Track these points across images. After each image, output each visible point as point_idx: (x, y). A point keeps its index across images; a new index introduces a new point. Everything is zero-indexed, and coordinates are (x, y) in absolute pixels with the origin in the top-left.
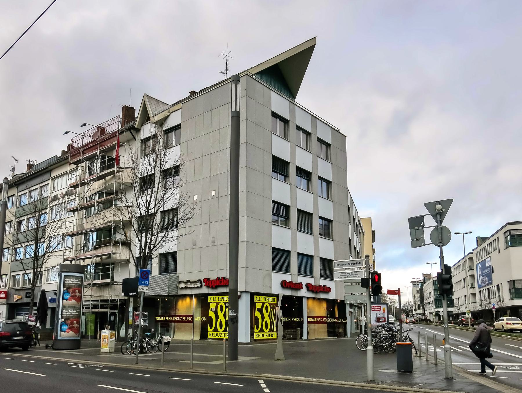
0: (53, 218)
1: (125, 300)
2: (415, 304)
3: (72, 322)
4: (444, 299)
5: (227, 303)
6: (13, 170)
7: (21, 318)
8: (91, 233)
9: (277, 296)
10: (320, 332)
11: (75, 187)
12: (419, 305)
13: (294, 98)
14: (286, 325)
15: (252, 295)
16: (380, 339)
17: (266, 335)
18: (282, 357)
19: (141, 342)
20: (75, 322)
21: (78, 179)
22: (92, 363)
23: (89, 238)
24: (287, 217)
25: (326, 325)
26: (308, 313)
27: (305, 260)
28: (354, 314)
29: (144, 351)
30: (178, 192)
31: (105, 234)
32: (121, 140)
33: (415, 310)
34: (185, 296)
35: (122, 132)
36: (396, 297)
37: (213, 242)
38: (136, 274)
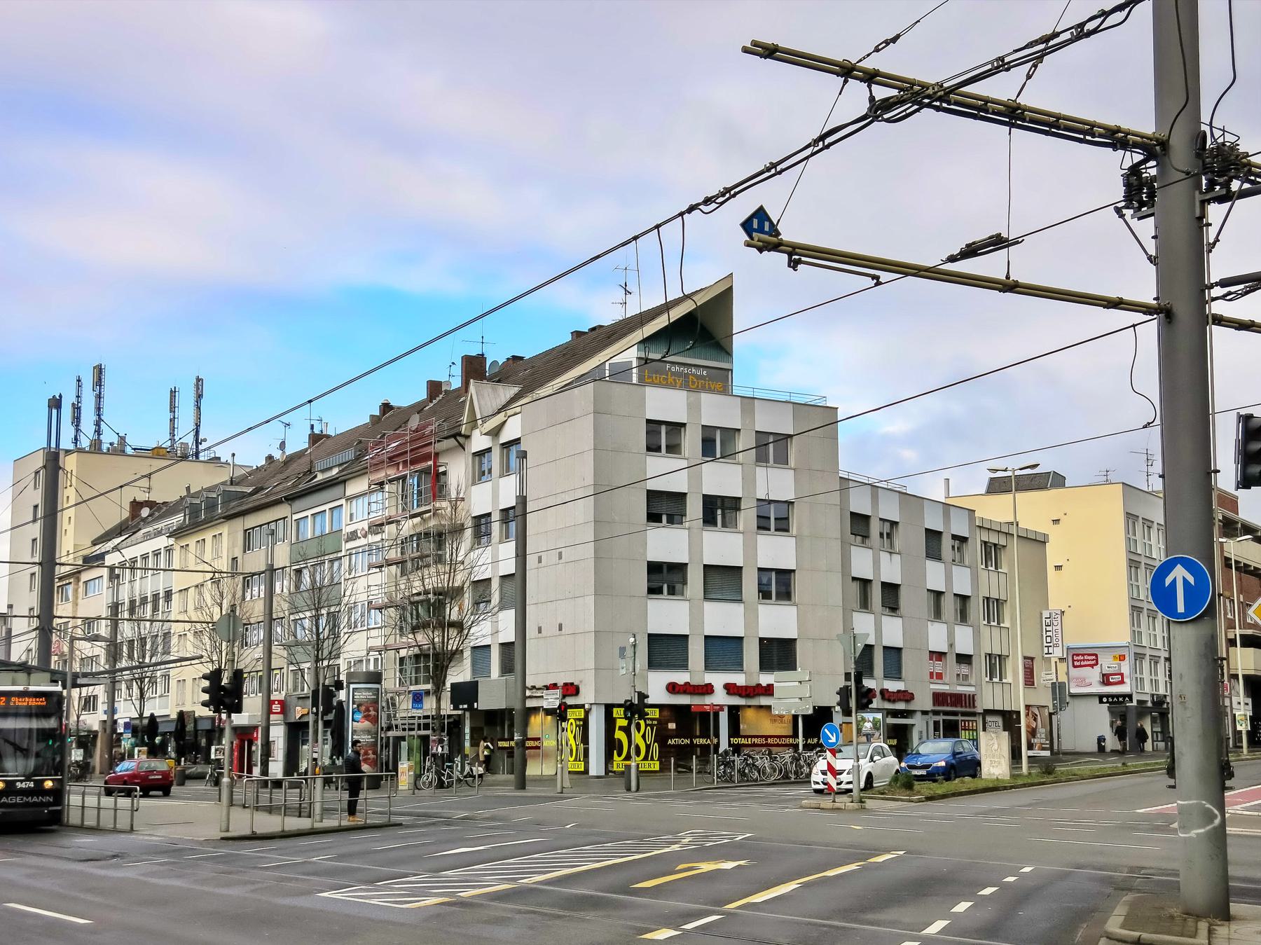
6: (282, 446)
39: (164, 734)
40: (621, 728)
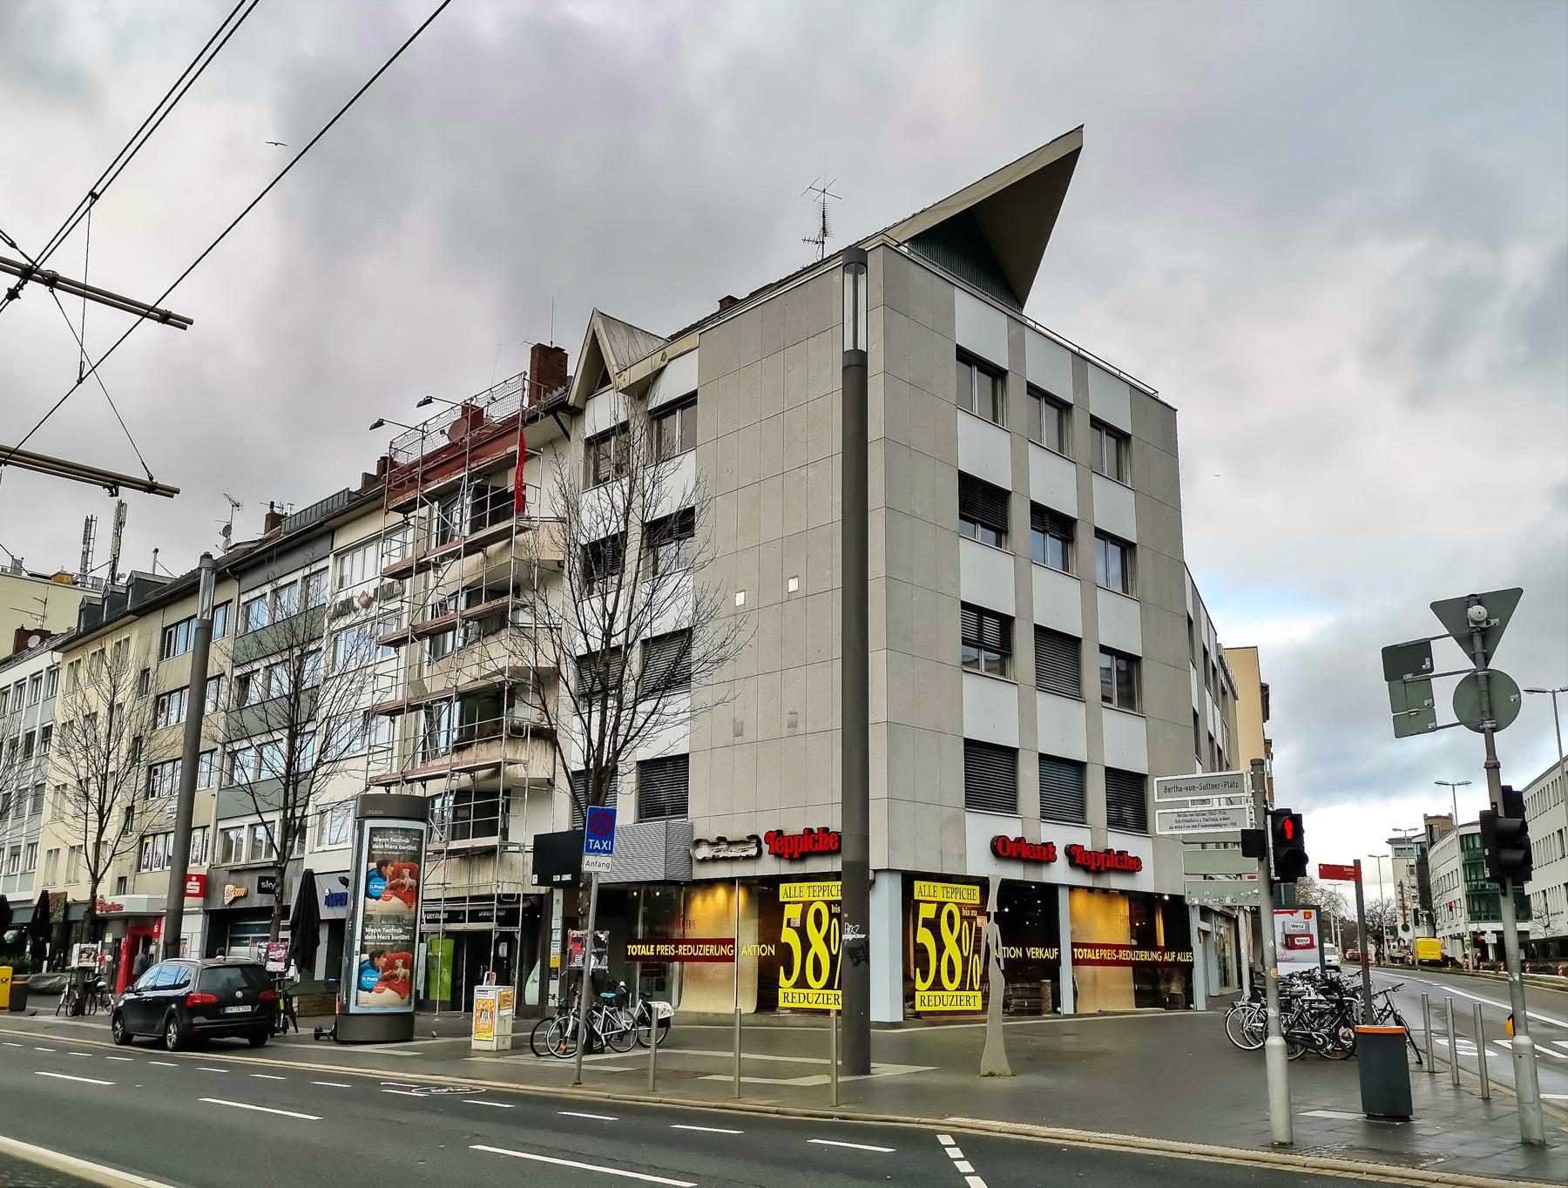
0: (340, 664)
1: (540, 896)
2: (1404, 908)
3: (391, 963)
4: (1504, 894)
5: (838, 903)
6: (227, 530)
7: (242, 953)
8: (444, 705)
9: (983, 883)
10: (1113, 993)
11: (401, 574)
12: (1416, 911)
13: (1021, 304)
14: (1013, 970)
15: (908, 879)
16: (1300, 1016)
17: (951, 999)
18: (1003, 1065)
19: (590, 1019)
20: (399, 963)
21: (409, 554)
22: (448, 1080)
23: (439, 721)
24: (1005, 649)
25: (1130, 969)
26: (1072, 933)
27: (1063, 775)
28: (1215, 938)
29: (596, 1045)
30: (690, 584)
31: (485, 708)
32: (528, 443)
33: (1405, 928)
34: (711, 884)
35: (533, 419)
36: (1347, 889)
37: (793, 725)
38: (574, 818)
39: (19, 927)
40: (928, 924)
